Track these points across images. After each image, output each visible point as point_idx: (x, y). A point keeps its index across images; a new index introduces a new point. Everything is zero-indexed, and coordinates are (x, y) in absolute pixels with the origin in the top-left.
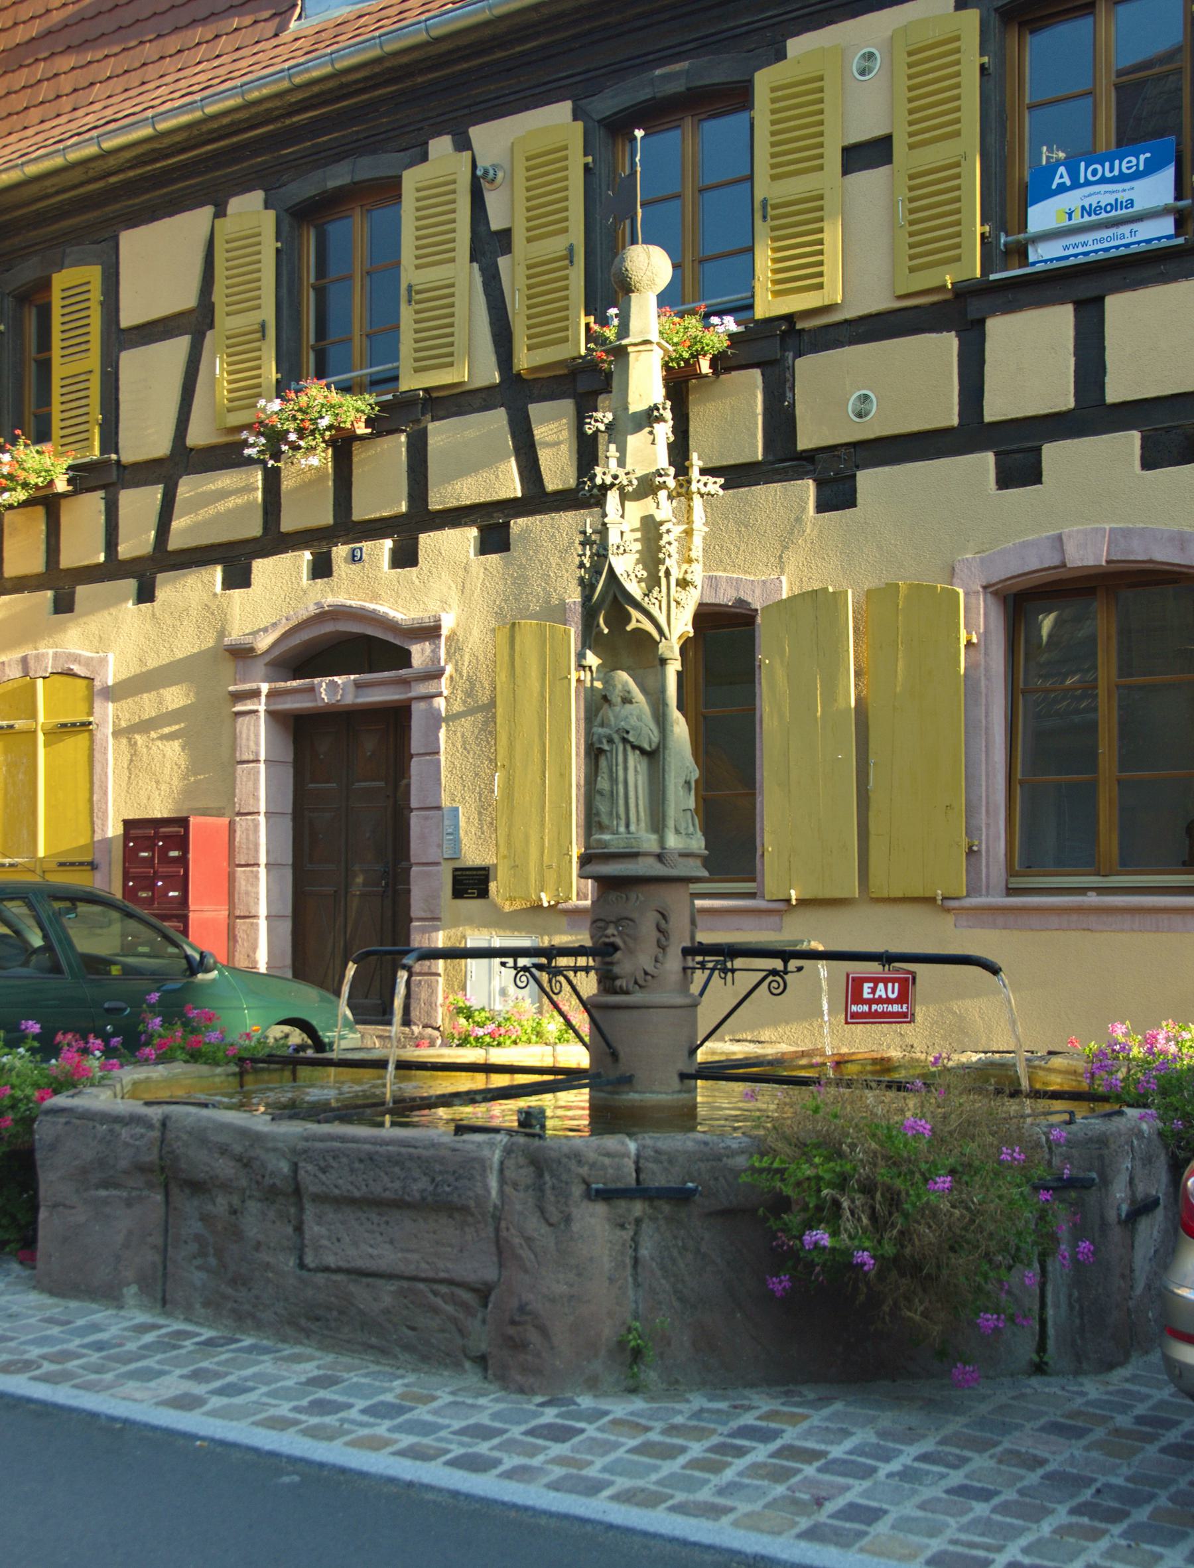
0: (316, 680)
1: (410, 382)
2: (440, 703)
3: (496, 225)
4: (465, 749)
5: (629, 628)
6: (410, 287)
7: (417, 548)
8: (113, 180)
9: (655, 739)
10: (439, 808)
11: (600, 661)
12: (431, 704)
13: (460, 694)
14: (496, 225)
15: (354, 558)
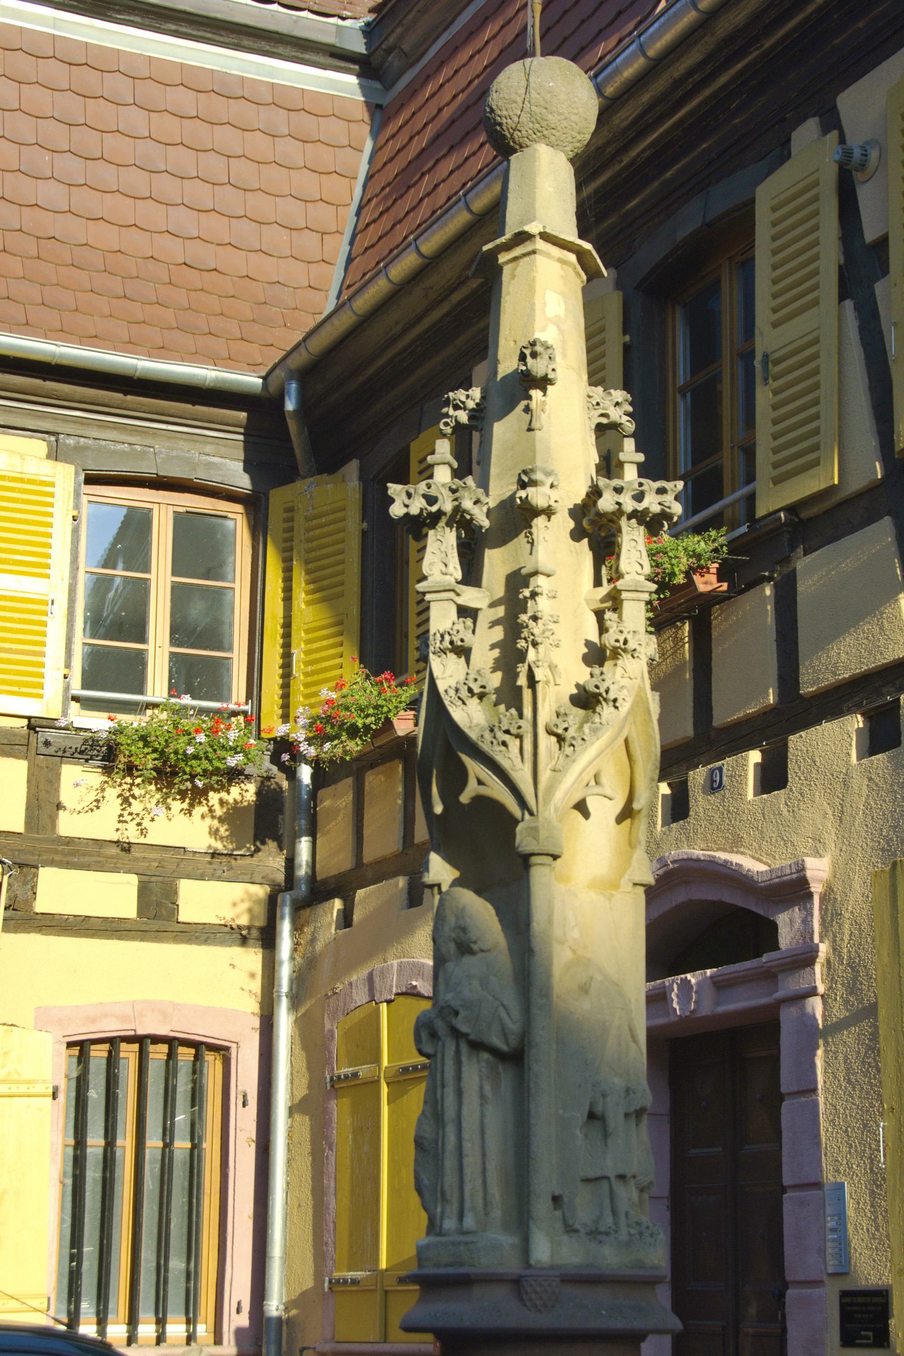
0: (667, 981)
1: (772, 500)
2: (816, 1006)
3: (870, 235)
4: (849, 1082)
6: (766, 356)
7: (786, 757)
8: (456, 297)
9: (514, 1027)
10: (817, 1185)
11: (456, 874)
12: (803, 1008)
13: (840, 990)
14: (870, 235)
15: (714, 786)
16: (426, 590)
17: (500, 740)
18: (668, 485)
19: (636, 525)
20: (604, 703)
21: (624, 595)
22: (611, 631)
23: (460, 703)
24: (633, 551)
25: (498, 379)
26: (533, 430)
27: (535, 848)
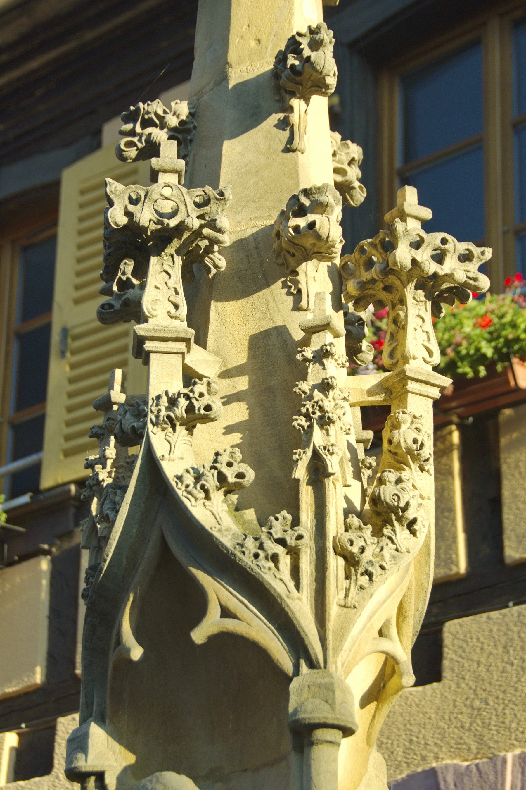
5: (199, 635)
6: (65, 332)
11: (131, 759)
16: (148, 334)
17: (270, 552)
18: (476, 251)
19: (423, 298)
20: (396, 523)
21: (411, 385)
22: (404, 427)
23: (202, 495)
24: (419, 330)
25: (230, 87)
26: (294, 151)
27: (317, 717)
